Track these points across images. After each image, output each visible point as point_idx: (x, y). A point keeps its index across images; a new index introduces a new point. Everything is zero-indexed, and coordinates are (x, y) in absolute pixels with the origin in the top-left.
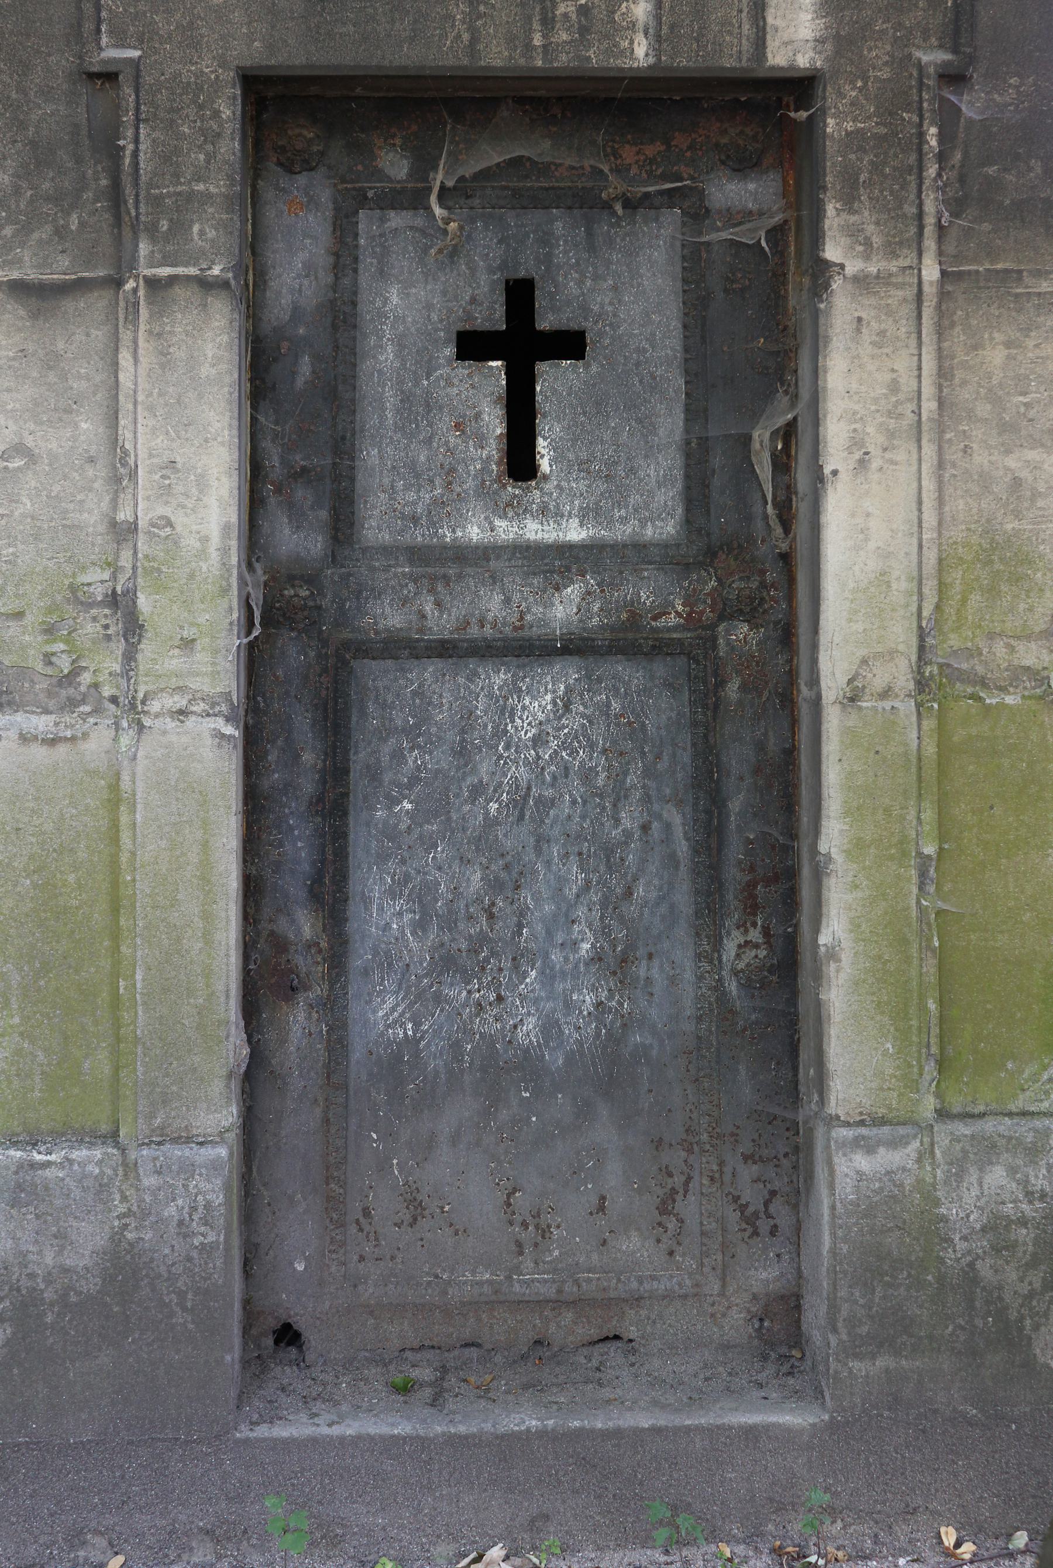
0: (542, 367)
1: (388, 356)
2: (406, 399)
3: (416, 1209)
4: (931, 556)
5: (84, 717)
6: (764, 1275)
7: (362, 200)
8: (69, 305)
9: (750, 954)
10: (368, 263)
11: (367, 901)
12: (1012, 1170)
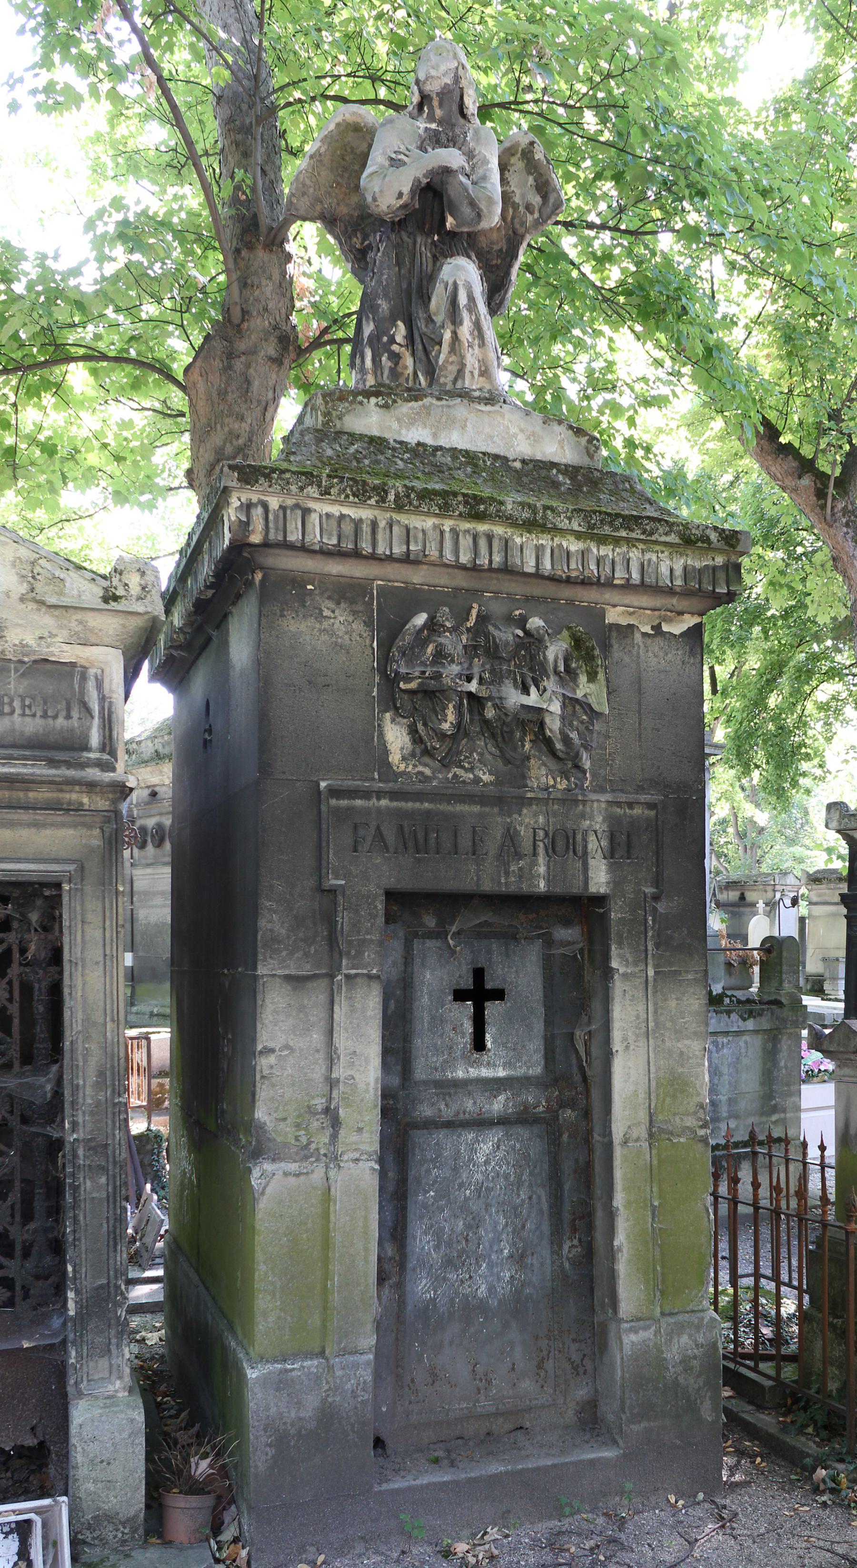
0: (488, 1004)
1: (425, 1000)
2: (433, 1018)
3: (434, 1377)
4: (653, 1084)
5: (312, 1163)
6: (582, 1393)
7: (416, 935)
8: (309, 985)
9: (574, 1251)
10: (417, 961)
11: (415, 1238)
12: (690, 1336)
